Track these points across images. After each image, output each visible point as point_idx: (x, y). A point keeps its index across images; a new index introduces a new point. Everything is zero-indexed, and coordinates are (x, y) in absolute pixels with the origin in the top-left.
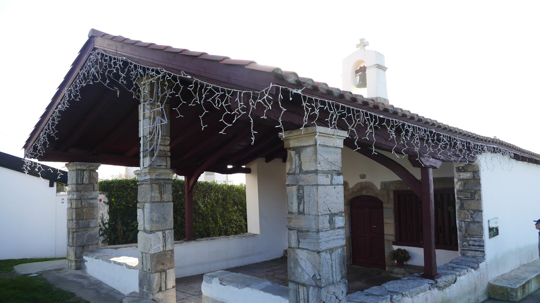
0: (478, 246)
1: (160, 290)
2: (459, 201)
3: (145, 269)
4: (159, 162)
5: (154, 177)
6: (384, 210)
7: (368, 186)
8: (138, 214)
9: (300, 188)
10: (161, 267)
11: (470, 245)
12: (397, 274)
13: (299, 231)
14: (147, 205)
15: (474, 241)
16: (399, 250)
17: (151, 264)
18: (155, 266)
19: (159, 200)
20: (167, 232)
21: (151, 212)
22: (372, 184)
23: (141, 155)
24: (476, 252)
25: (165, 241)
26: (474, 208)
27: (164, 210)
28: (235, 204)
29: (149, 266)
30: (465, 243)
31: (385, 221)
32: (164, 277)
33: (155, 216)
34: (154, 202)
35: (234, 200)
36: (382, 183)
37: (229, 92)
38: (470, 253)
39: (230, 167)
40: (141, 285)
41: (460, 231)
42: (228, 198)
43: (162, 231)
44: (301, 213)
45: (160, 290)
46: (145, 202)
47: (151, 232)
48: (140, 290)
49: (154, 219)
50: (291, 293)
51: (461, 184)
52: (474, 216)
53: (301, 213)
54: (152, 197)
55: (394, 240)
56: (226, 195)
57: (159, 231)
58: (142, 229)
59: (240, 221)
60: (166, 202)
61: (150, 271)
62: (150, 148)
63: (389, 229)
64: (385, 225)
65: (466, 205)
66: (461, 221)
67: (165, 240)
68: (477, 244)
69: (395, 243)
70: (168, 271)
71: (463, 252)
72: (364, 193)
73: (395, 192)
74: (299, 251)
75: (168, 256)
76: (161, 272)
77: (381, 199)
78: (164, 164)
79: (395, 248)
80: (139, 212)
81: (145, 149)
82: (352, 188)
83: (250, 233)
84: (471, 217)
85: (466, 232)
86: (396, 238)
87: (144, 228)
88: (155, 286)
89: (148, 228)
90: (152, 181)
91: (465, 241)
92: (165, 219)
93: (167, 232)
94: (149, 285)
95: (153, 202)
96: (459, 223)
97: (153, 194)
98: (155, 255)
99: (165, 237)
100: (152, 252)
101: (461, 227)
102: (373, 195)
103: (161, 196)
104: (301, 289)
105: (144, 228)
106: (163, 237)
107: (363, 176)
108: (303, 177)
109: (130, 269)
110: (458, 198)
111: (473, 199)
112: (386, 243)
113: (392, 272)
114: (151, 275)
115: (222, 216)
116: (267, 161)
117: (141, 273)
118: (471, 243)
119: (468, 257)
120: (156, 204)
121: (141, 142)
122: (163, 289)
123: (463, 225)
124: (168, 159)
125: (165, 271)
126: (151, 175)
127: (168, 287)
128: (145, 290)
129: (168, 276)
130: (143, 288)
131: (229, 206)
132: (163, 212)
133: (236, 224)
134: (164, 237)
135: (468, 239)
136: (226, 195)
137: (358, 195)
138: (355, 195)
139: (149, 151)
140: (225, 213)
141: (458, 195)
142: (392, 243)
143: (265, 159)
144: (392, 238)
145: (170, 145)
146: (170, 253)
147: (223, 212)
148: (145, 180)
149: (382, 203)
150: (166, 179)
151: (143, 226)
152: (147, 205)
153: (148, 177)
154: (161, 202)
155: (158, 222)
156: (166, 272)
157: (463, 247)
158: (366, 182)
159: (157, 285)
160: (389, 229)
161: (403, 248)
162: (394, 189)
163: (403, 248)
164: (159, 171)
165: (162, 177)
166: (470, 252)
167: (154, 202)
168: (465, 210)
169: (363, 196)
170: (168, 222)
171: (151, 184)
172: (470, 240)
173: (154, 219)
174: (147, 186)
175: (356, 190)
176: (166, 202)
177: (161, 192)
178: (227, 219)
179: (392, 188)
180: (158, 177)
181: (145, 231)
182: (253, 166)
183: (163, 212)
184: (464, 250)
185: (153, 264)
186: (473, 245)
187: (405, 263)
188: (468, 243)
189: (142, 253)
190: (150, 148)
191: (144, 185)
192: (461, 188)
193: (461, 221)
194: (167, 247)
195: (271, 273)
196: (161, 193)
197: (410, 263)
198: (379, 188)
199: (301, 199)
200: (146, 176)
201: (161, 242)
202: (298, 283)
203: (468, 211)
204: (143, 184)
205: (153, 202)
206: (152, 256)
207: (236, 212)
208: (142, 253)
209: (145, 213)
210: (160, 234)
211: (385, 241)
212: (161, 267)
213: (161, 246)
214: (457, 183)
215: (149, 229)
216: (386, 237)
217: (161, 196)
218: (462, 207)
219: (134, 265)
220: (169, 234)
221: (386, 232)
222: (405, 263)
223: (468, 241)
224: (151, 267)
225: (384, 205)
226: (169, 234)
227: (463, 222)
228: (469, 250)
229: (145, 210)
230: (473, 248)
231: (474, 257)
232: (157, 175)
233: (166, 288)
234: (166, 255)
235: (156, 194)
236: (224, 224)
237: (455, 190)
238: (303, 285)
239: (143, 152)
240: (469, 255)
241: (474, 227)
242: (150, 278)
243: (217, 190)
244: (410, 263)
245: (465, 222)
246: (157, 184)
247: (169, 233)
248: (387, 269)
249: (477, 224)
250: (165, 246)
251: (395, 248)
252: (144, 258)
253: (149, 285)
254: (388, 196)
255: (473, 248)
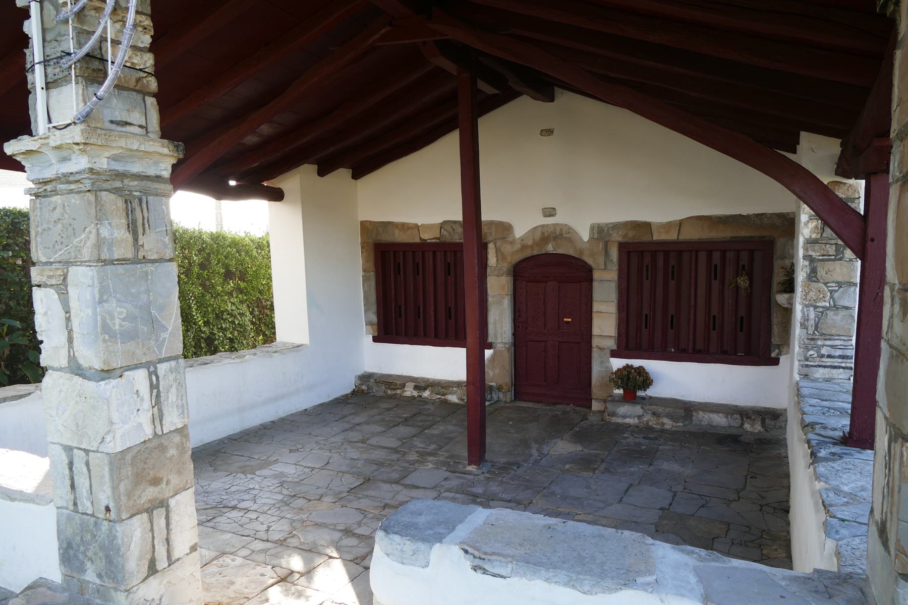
0: (840, 357)
1: (152, 570)
2: (807, 263)
3: (86, 505)
4: (118, 109)
5: (103, 164)
6: (595, 284)
7: (562, 234)
8: (38, 306)
10: (151, 493)
11: (822, 356)
12: (624, 417)
14: (83, 280)
15: (832, 346)
16: (628, 367)
17: (115, 488)
18: (129, 495)
19: (129, 255)
20: (162, 368)
21: (101, 302)
22: (570, 228)
23: (37, 78)
24: (835, 371)
25: (157, 402)
26: (840, 279)
27: (148, 291)
28: (228, 275)
29: (104, 497)
30: (811, 352)
31: (596, 307)
32: (163, 522)
33: (118, 311)
34: (112, 262)
35: (226, 267)
36: (592, 228)
38: (820, 373)
39: (232, 183)
40: (70, 555)
41: (803, 326)
42: (214, 262)
43: (146, 365)
45: (152, 570)
46: (68, 263)
47: (107, 373)
48: (65, 576)
49: (116, 325)
51: (816, 227)
52: (836, 295)
54: (100, 243)
55: (615, 347)
56: (209, 254)
57: (136, 367)
58: (64, 363)
59: (242, 315)
60: (154, 261)
61: (113, 515)
62: (80, 45)
63: (605, 324)
64: (594, 315)
65: (821, 272)
66: (807, 306)
67: (158, 396)
68: (838, 353)
69: (614, 354)
70: (172, 502)
71: (805, 370)
72: (550, 248)
73: (622, 246)
75: (172, 452)
76: (149, 511)
77: (589, 261)
78: (136, 117)
79: (617, 363)
81: (54, 51)
83: (284, 344)
84: (831, 297)
85: (816, 328)
86: (619, 344)
87: (72, 359)
88: (134, 561)
89: (90, 356)
91: (812, 349)
92: (154, 324)
93: (162, 368)
94: (109, 561)
95: (105, 262)
96: (802, 311)
97: (105, 232)
98: (129, 457)
99: (157, 387)
100: (116, 445)
101: (806, 319)
102: (571, 252)
103: (136, 240)
105: (72, 359)
106: (152, 387)
107: (550, 212)
109: (13, 500)
110: (805, 257)
111: (841, 259)
112: (595, 354)
113: (613, 414)
114: (119, 528)
115: (201, 305)
116: (322, 173)
117: (69, 519)
118: (824, 351)
119: (815, 380)
120: (120, 269)
121: (32, 27)
122: (162, 563)
123: (812, 315)
124: (151, 101)
125: (163, 504)
126: (91, 157)
127: (176, 554)
128: (90, 576)
129: (174, 517)
130: (84, 571)
131: (217, 280)
132: (144, 297)
133: (233, 322)
134: (154, 386)
135: (820, 343)
136: (209, 254)
137: (535, 253)
138: (528, 253)
139: (74, 58)
140: (208, 297)
141: (806, 249)
142: (608, 354)
143: (315, 167)
144: (612, 344)
145: (152, 49)
146: (177, 439)
147: (203, 296)
148: (66, 178)
149: (589, 270)
150: (148, 178)
151: (64, 352)
152: (83, 280)
153: (79, 163)
154: (135, 261)
155: (129, 336)
156: (168, 507)
157: (807, 360)
159: (140, 558)
160: (605, 324)
161: (636, 363)
162: (620, 239)
163: (636, 363)
164: (122, 143)
165: (136, 168)
166: (821, 370)
167: (112, 262)
168: (818, 281)
169: (547, 254)
170: (165, 335)
171: (95, 191)
172: (823, 346)
173: (116, 325)
174: (75, 199)
175: (530, 243)
176: (154, 261)
177: (134, 222)
178: (213, 310)
179: (617, 237)
180: (119, 167)
181: (76, 369)
182: (290, 182)
183: (144, 297)
184: (807, 366)
185: (122, 487)
186: (829, 356)
187: (640, 393)
188: (818, 352)
189: (68, 449)
190: (80, 45)
191: (57, 199)
192: (814, 236)
193: (807, 306)
194: (167, 420)
195: (355, 436)
196: (132, 227)
197: (651, 392)
198: (585, 237)
200: (65, 159)
201: (147, 404)
203: (825, 284)
204: (55, 192)
205: (105, 262)
206: (117, 460)
207: (230, 294)
208: (68, 449)
209: (74, 304)
210: (140, 378)
211: (595, 350)
212: (151, 493)
213: (145, 419)
214: (806, 224)
215: (98, 365)
216: (595, 342)
217: (136, 240)
218: (813, 276)
219: (28, 486)
220: (171, 377)
221: (596, 331)
223: (819, 348)
224: (116, 497)
225: (596, 275)
226: (171, 377)
227: (812, 309)
228: (820, 366)
229: (73, 292)
230: (829, 362)
231: (828, 380)
232: (114, 158)
233: (169, 557)
234: (162, 448)
235: (116, 231)
236: (207, 323)
237: (801, 240)
239: (46, 62)
240: (817, 376)
241: (835, 317)
242: (112, 537)
243: (188, 242)
244: (651, 392)
245: (816, 307)
246: (116, 191)
247: (171, 371)
248: (596, 406)
249: (843, 313)
250: (158, 417)
251: (617, 363)
252: (79, 466)
253: (109, 561)
255: (829, 362)
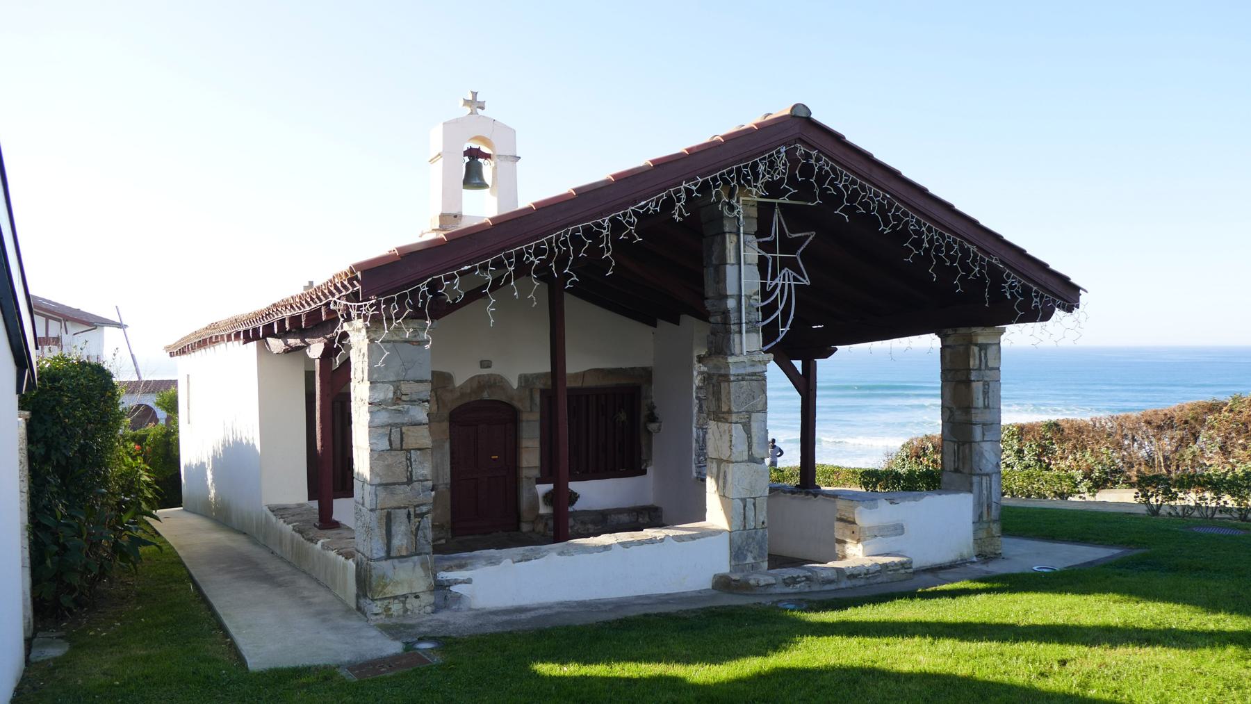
7: (496, 383)
9: (986, 384)
13: (984, 425)
36: (520, 377)
37: (745, 167)
44: (986, 407)
50: (975, 488)
53: (986, 407)
63: (530, 459)
72: (485, 395)
73: (543, 392)
74: (983, 444)
80: (448, 481)
82: (461, 387)
90: (333, 321)
102: (504, 399)
104: (984, 479)
107: (485, 364)
108: (988, 372)
138: (466, 400)
144: (536, 473)
158: (490, 375)
160: (530, 459)
179: (539, 385)
187: (570, 509)
197: (578, 506)
199: (986, 393)
202: (981, 475)
222: (570, 509)
238: (987, 475)
254: (532, 399)
